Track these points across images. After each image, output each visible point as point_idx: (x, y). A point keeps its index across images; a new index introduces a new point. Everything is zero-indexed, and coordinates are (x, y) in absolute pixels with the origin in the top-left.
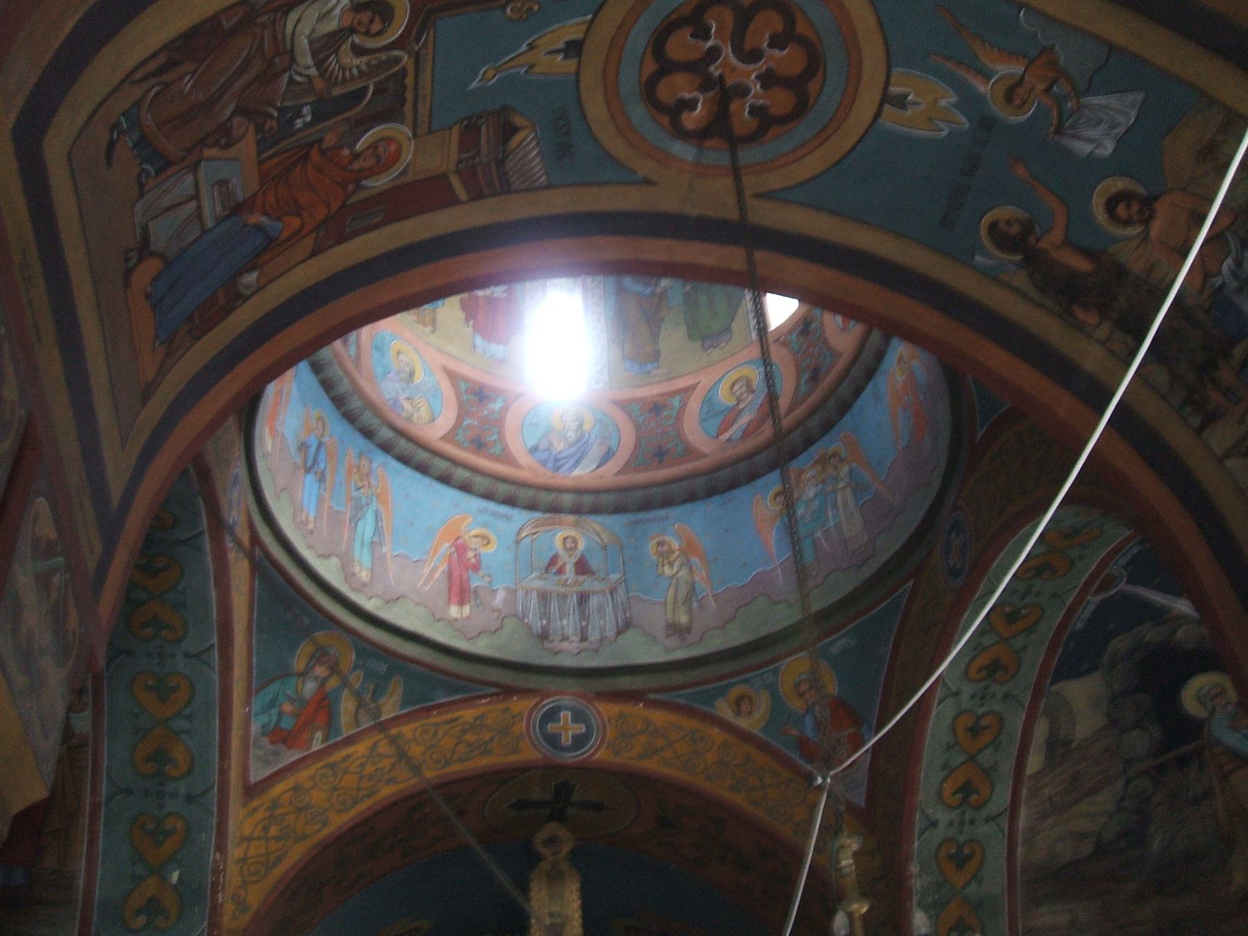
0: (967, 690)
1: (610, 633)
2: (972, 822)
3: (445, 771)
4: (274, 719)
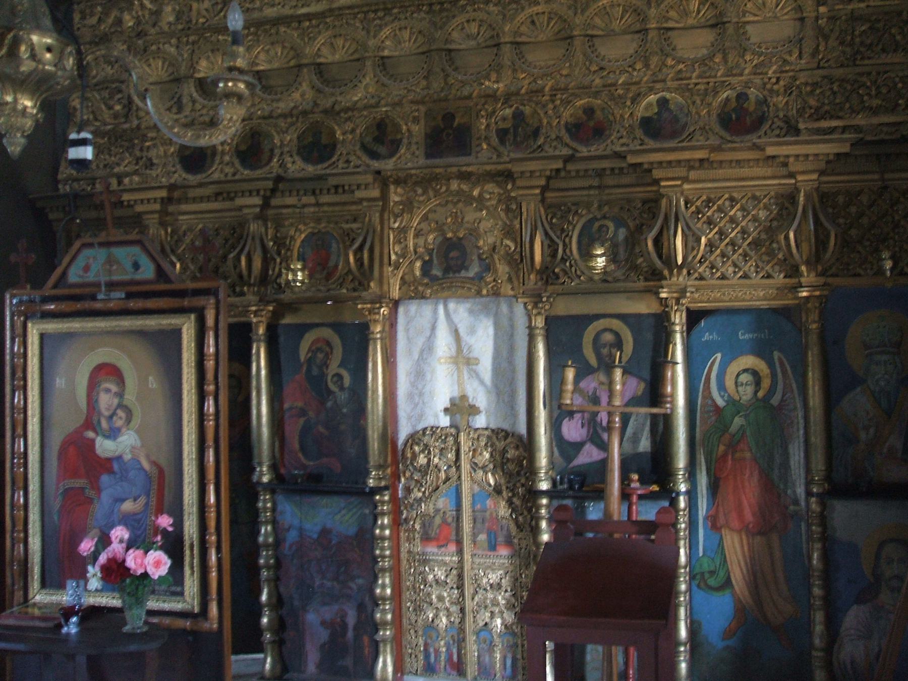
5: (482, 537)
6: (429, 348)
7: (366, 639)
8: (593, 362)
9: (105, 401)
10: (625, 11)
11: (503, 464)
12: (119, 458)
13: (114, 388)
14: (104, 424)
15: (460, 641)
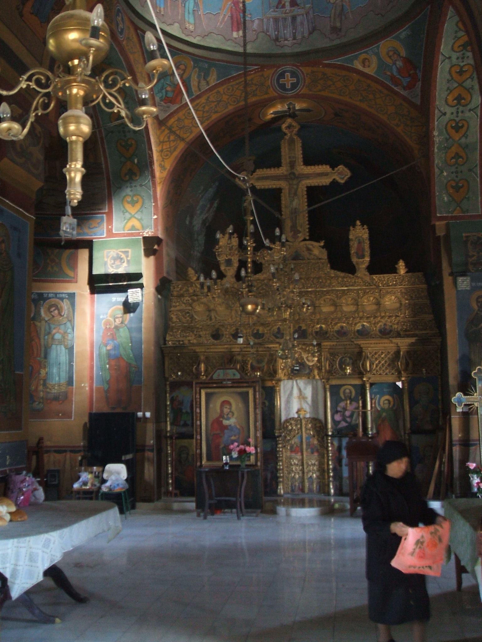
0: (454, 56)
1: (306, 35)
2: (462, 112)
3: (238, 105)
4: (164, 94)
5: (309, 450)
6: (291, 394)
7: (274, 483)
8: (343, 397)
9: (226, 410)
10: (352, 299)
11: (315, 428)
12: (230, 425)
13: (228, 407)
14: (225, 416)
15: (303, 482)
